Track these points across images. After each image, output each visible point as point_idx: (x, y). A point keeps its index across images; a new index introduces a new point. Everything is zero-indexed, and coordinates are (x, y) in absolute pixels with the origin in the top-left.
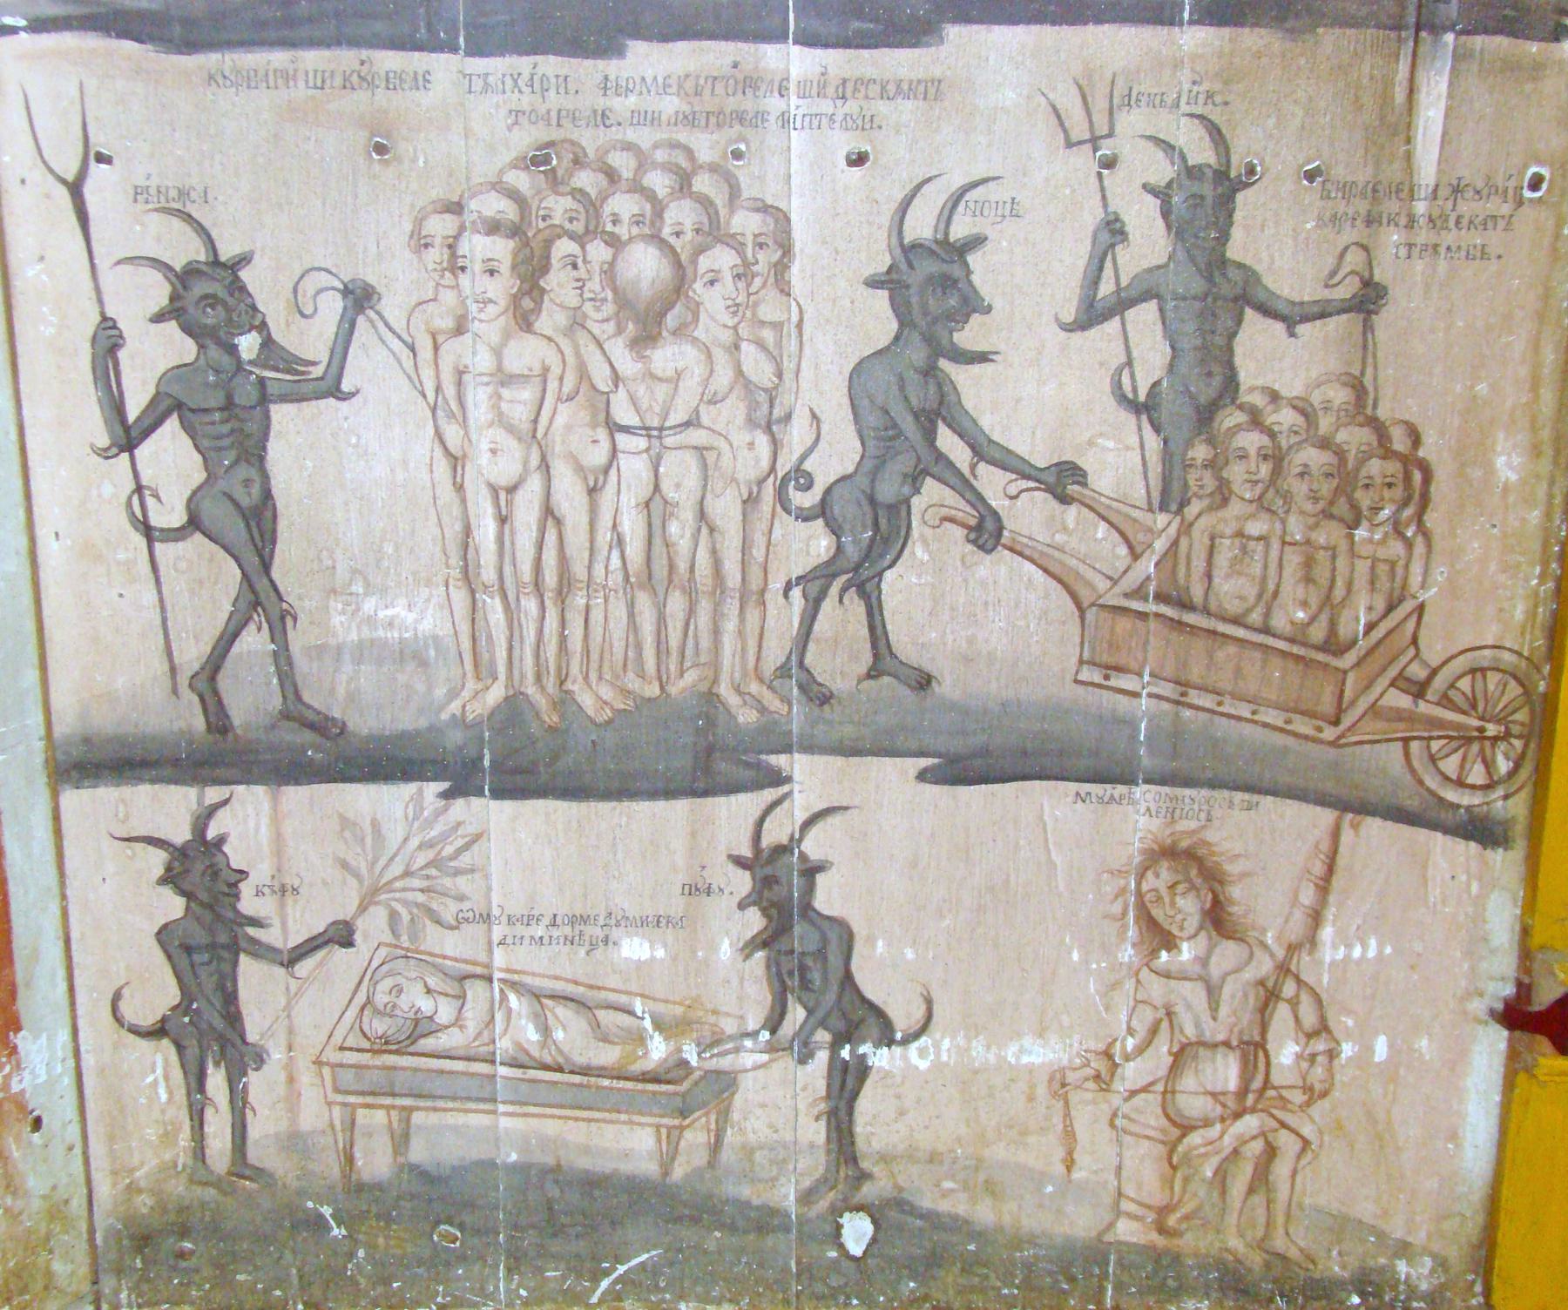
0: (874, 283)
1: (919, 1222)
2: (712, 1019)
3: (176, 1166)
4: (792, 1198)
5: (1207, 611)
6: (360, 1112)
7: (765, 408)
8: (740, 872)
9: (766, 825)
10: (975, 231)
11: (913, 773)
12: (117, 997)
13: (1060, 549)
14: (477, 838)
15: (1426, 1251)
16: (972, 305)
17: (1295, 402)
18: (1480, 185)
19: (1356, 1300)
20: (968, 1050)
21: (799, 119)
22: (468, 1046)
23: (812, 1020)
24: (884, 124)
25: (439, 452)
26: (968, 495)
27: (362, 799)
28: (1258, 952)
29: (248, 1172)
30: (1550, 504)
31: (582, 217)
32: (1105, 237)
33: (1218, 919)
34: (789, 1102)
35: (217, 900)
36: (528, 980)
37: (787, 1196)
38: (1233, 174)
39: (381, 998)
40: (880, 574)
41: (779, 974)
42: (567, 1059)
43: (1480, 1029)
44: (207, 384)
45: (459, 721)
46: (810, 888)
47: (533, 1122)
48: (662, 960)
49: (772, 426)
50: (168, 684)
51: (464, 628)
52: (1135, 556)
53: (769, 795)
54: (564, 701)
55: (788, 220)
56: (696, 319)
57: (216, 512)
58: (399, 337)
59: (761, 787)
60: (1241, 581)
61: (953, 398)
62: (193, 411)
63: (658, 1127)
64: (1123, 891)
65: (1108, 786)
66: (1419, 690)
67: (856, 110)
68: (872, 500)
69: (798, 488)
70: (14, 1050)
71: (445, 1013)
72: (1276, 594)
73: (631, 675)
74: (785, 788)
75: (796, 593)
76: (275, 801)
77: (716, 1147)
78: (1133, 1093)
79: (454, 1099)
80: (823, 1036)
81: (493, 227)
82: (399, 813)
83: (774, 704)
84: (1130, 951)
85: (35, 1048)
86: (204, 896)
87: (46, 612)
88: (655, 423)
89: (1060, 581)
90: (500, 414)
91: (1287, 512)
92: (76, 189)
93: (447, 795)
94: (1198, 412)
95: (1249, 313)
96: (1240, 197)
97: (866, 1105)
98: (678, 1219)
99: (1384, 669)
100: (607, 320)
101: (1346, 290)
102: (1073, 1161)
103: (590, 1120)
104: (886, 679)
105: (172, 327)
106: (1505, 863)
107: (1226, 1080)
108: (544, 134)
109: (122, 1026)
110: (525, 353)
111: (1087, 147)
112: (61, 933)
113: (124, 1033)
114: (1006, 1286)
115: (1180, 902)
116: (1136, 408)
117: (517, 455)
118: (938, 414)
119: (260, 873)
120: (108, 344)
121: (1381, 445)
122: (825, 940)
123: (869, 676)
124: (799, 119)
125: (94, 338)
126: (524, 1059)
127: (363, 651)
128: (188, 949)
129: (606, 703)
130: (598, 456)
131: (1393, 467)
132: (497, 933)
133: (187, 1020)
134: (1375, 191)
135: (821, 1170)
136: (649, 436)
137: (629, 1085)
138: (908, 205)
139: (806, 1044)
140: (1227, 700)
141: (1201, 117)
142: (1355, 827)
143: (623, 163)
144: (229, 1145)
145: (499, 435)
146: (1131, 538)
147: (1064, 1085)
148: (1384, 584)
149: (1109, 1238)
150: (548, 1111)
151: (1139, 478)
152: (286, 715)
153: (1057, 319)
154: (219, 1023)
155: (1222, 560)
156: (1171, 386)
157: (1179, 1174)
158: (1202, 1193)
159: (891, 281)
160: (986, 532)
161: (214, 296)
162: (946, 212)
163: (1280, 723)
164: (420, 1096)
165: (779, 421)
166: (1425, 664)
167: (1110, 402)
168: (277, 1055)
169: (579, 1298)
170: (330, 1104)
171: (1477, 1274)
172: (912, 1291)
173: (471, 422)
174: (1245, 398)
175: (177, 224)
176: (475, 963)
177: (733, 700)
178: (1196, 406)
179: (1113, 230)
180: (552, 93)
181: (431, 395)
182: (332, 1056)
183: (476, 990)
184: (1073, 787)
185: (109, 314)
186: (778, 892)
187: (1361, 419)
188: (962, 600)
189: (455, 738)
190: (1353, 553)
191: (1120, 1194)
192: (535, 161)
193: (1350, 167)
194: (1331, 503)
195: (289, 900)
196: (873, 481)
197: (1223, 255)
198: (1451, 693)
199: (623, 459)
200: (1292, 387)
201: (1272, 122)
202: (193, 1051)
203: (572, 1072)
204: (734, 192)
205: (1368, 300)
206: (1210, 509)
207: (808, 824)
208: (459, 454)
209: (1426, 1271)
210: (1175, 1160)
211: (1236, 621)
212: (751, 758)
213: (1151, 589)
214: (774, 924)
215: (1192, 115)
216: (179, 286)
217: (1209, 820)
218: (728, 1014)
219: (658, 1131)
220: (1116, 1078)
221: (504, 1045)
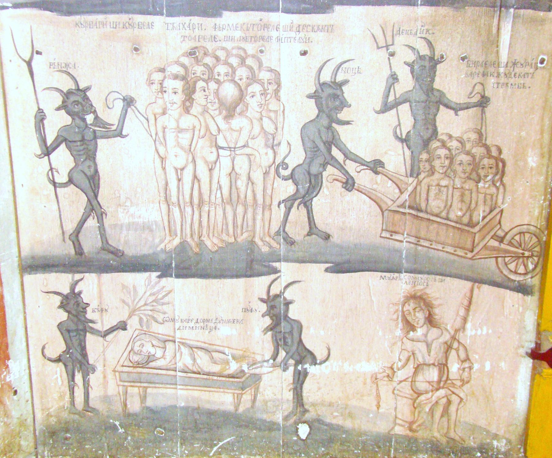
0: (310, 97)
2: (253, 356)
3: (64, 407)
4: (281, 418)
5: (426, 212)
6: (129, 388)
8: (263, 304)
9: (272, 287)
10: (345, 78)
11: (323, 269)
12: (43, 348)
14: (170, 292)
15: (503, 437)
16: (344, 104)
17: (458, 139)
18: (522, 62)
20: (342, 366)
23: (288, 356)
25: (157, 156)
26: (343, 171)
27: (129, 278)
28: (445, 332)
29: (89, 410)
30: (547, 175)
31: (207, 73)
32: (391, 80)
33: (430, 320)
35: (78, 313)
36: (188, 342)
37: (279, 418)
38: (436, 58)
39: (136, 348)
40: (312, 199)
41: (276, 340)
42: (202, 370)
43: (523, 359)
44: (75, 132)
45: (164, 251)
46: (287, 310)
47: (190, 392)
49: (273, 146)
51: (166, 218)
52: (401, 193)
53: (273, 277)
54: (201, 244)
56: (247, 109)
60: (439, 201)
61: (337, 137)
63: (234, 394)
64: (397, 311)
65: (392, 274)
66: (501, 240)
68: (309, 173)
69: (283, 169)
70: (7, 367)
71: (159, 353)
72: (451, 206)
73: (224, 234)
74: (278, 274)
75: (282, 206)
77: (254, 401)
78: (401, 382)
79: (162, 384)
82: (143, 283)
83: (274, 244)
86: (74, 312)
87: (19, 212)
88: (233, 146)
89: (375, 202)
90: (178, 143)
91: (455, 177)
92: (29, 63)
93: (160, 277)
95: (441, 107)
96: (438, 66)
98: (241, 426)
99: (489, 233)
100: (216, 110)
104: (314, 236)
106: (531, 301)
107: (433, 377)
108: (193, 44)
110: (187, 121)
111: (385, 49)
113: (46, 360)
114: (356, 449)
115: (417, 314)
116: (402, 141)
118: (332, 143)
119: (94, 304)
120: (40, 118)
121: (488, 153)
122: (292, 328)
123: (308, 235)
126: (186, 370)
127: (129, 227)
128: (69, 331)
129: (215, 244)
130: (212, 157)
131: (492, 161)
132: (177, 325)
133: (68, 356)
134: (486, 64)
136: (231, 151)
137: (224, 379)
138: (322, 69)
140: (434, 243)
141: (425, 38)
142: (479, 288)
143: (221, 54)
144: (83, 400)
145: (178, 150)
146: (400, 186)
148: (489, 202)
150: (195, 388)
152: (103, 249)
153: (374, 109)
154: (79, 357)
155: (432, 194)
156: (414, 133)
157: (417, 410)
158: (425, 417)
159: (315, 96)
160: (349, 184)
161: (78, 101)
162: (335, 72)
163: (452, 252)
164: (150, 383)
165: (276, 145)
166: (503, 230)
168: (100, 368)
169: (206, 454)
170: (118, 385)
171: (521, 445)
172: (323, 451)
174: (440, 137)
175: (65, 76)
176: (169, 336)
177: (260, 243)
178: (423, 140)
179: (394, 78)
180: (197, 29)
182: (119, 368)
184: (380, 274)
186: (276, 311)
187: (481, 144)
188: (340, 208)
189: (163, 257)
190: (478, 192)
191: (396, 417)
192: (191, 54)
194: (470, 174)
195: (104, 313)
196: (309, 166)
198: (512, 241)
200: (456, 133)
201: (449, 40)
202: (70, 367)
203: (203, 374)
205: (483, 102)
206: (428, 176)
207: (286, 287)
208: (164, 157)
209: (503, 444)
210: (415, 405)
211: (437, 216)
213: (407, 204)
214: (274, 322)
215: (421, 38)
216: (65, 98)
218: (258, 354)
219: (234, 395)
221: (180, 365)
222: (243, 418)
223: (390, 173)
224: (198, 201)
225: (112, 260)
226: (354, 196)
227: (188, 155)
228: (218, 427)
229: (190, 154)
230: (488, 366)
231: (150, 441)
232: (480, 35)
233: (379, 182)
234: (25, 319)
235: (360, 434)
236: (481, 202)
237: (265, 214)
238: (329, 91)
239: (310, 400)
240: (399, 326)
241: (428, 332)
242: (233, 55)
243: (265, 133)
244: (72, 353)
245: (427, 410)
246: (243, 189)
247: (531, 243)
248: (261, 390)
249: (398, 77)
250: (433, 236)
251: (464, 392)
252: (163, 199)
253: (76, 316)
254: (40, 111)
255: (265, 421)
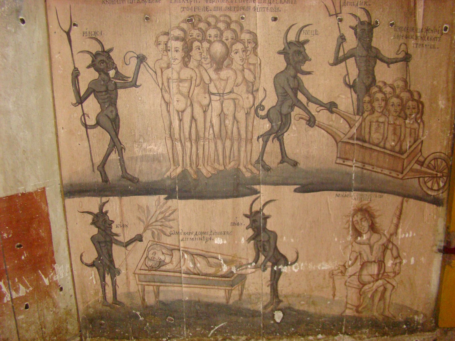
0: (280, 53)
1: (295, 313)
2: (239, 260)
3: (99, 301)
4: (261, 308)
5: (369, 143)
6: (146, 287)
7: (251, 88)
8: (247, 219)
9: (253, 205)
10: (306, 39)
11: (293, 190)
12: (81, 256)
13: (331, 126)
14: (175, 211)
15: (422, 313)
16: (306, 59)
17: (391, 86)
18: (432, 29)
19: (405, 326)
20: (308, 266)
21: (259, 9)
22: (174, 269)
23: (266, 259)
24: (281, 10)
25: (163, 102)
26: (306, 111)
27: (144, 200)
28: (383, 236)
29: (117, 303)
30: (452, 114)
31: (201, 36)
32: (340, 40)
33: (373, 228)
34: (261, 282)
35: (106, 229)
36: (190, 250)
37: (260, 307)
38: (372, 24)
39: (150, 256)
40: (283, 134)
41: (257, 247)
42: (201, 272)
43: (436, 254)
44: (101, 85)
45: (169, 178)
46: (265, 223)
47: (192, 289)
48: (226, 244)
49: (253, 92)
50: (92, 168)
51: (170, 151)
52: (351, 127)
53: (254, 197)
54: (198, 171)
55: (256, 36)
56: (232, 63)
57: (104, 120)
58: (152, 70)
59: (251, 194)
60: (378, 134)
61: (302, 84)
62: (97, 92)
63: (225, 290)
64: (348, 221)
65: (344, 192)
66: (422, 164)
67: (274, 6)
68: (281, 114)
69: (260, 110)
70: (54, 269)
71: (168, 260)
72: (387, 138)
73: (216, 164)
74: (258, 195)
75: (261, 140)
76: (120, 200)
77: (241, 294)
78: (351, 276)
79: (171, 283)
80: (269, 264)
81: (177, 39)
82: (154, 204)
83: (255, 171)
84: (350, 237)
85: (60, 269)
86: (102, 227)
87: (60, 149)
88: (222, 92)
89: (331, 135)
90: (179, 90)
91: (389, 115)
92: (68, 34)
93: (166, 199)
94: (366, 88)
95: (378, 61)
96: (374, 30)
97: (281, 282)
98: (231, 314)
99: (414, 158)
100: (208, 64)
101: (401, 56)
102: (335, 295)
103: (207, 288)
104: (285, 164)
105: (92, 69)
106: (442, 210)
107: (374, 271)
108: (190, 13)
109: (83, 263)
110: (186, 73)
111: (335, 16)
112: (66, 238)
113: (84, 265)
114: (317, 328)
115: (363, 223)
116: (350, 86)
117: (184, 102)
118: (298, 89)
119: (117, 221)
120: (76, 75)
121: (412, 97)
122: (269, 237)
123: (281, 163)
124: (259, 9)
125: (72, 74)
126: (189, 272)
127: (143, 158)
128: (99, 243)
129: (209, 172)
130: (206, 102)
131: (415, 103)
132: (181, 237)
133: (99, 262)
134: (407, 29)
135: (269, 300)
136: (220, 96)
137: (217, 278)
138: (288, 31)
139: (265, 266)
140: (375, 167)
141: (364, 8)
142: (407, 201)
143: (212, 20)
144: (112, 295)
145: (179, 96)
146: (349, 122)
147: (333, 275)
148: (413, 135)
149: (344, 314)
150: (196, 286)
151: (351, 106)
152: (123, 177)
153: (328, 62)
154: (108, 263)
155: (373, 129)
156: (359, 80)
157: (362, 297)
158: (368, 301)
159: (284, 52)
160: (311, 122)
161: (104, 60)
162: (298, 33)
163: (388, 174)
164: (162, 282)
165: (255, 91)
166: (423, 157)
167: (343, 85)
168: (123, 271)
169: (206, 336)
170: (138, 285)
171: (433, 318)
172: (293, 331)
173: (172, 93)
174: (378, 84)
175: (94, 41)
176: (175, 246)
177: (244, 170)
178: (365, 86)
179: (342, 38)
180: (193, 2)
181: (161, 85)
182: (138, 271)
183: (176, 253)
184: (335, 192)
185: (76, 67)
186: (258, 224)
187: (406, 90)
188: (305, 141)
189: (169, 182)
190: (406, 127)
191: (347, 303)
192: (188, 21)
193: (401, 23)
194: (400, 113)
195: (125, 228)
196: (281, 107)
197: (371, 44)
198: (430, 165)
199: (213, 103)
200: (389, 82)
201: (381, 10)
202: (102, 270)
203: (202, 275)
204: (242, 28)
205: (407, 58)
206: (370, 114)
207: (265, 205)
208: (168, 102)
209: (421, 318)
210: (361, 293)
211: (377, 145)
212: (249, 187)
213: (355, 137)
214: (256, 233)
215: (361, 8)
216: (94, 58)
217: (370, 200)
218: (244, 259)
219: (225, 291)
220: (347, 272)
221: (184, 268)
222: (233, 308)
223: (342, 112)
224: (195, 137)
225: (130, 185)
226: (315, 132)
227: (187, 100)
228: (214, 316)
229: (189, 100)
230: (412, 261)
231: (163, 327)
232: (403, 8)
233: (334, 119)
234: (67, 233)
235: (321, 317)
236: (407, 135)
237: (248, 146)
238: (294, 48)
239: (283, 293)
240: (350, 233)
241: (370, 237)
242: (220, 21)
243: (246, 82)
244: (102, 260)
245: (369, 296)
246: (230, 127)
247: (442, 167)
248: (246, 286)
249: (346, 38)
250: (374, 161)
251: (395, 281)
252: (168, 136)
253: (104, 231)
254: (76, 69)
255: (249, 310)
